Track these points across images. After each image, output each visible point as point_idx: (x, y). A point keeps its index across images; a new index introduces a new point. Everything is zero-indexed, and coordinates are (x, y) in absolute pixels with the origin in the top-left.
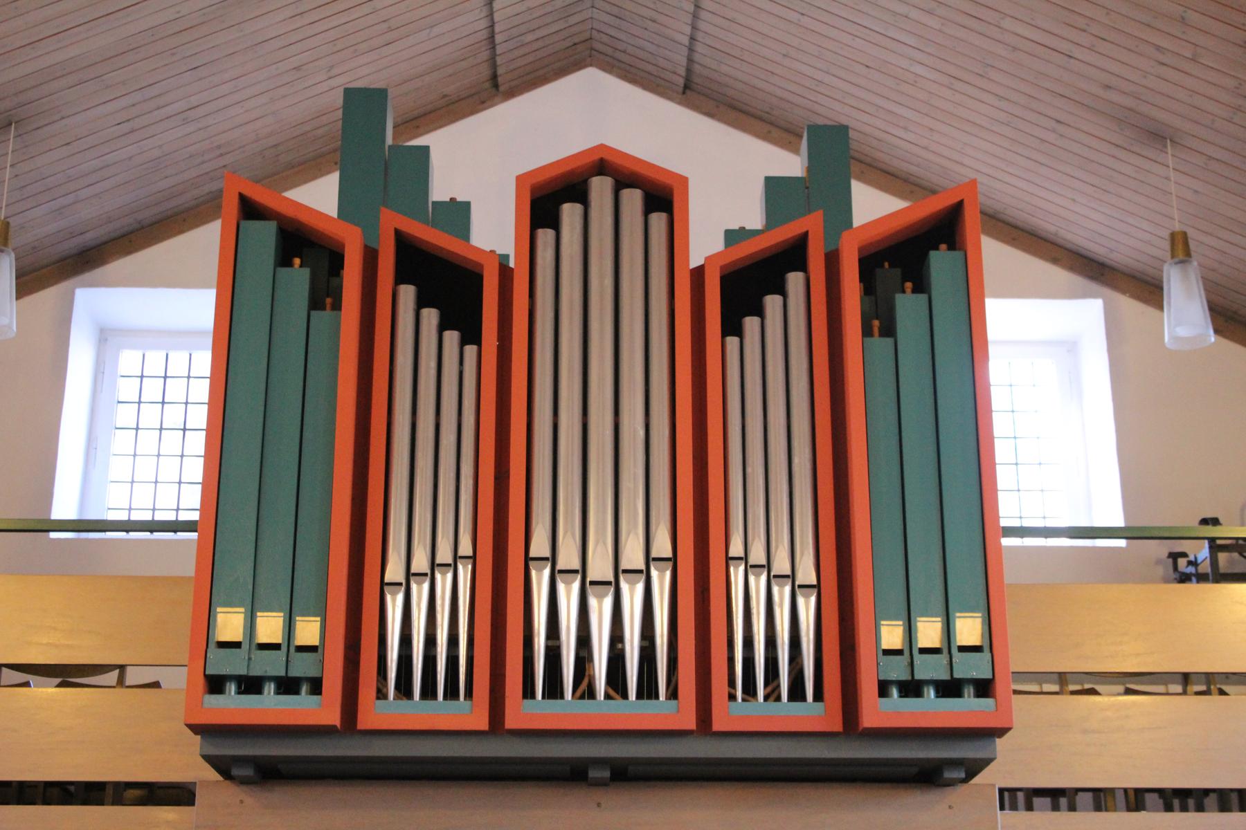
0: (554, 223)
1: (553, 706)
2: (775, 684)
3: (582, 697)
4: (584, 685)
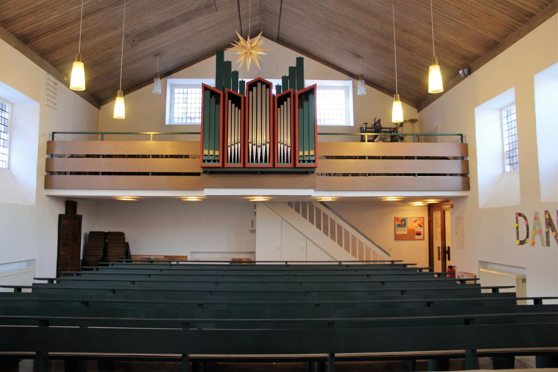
4: (257, 160)
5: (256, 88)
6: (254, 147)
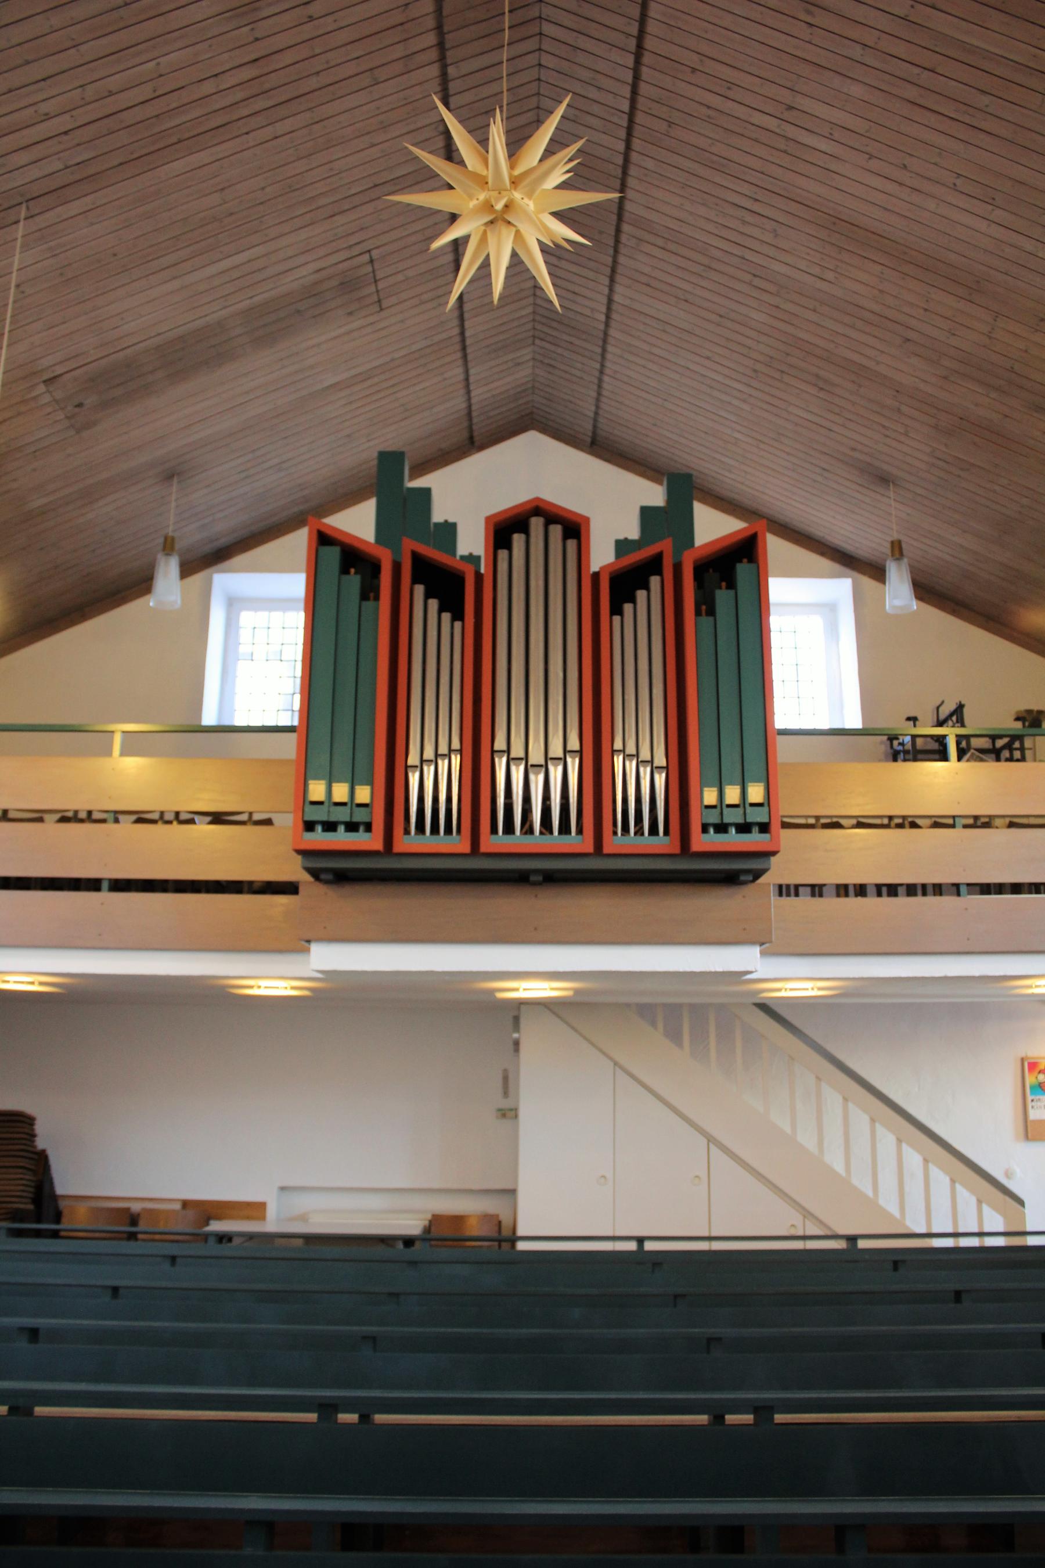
0: (508, 546)
1: (509, 839)
2: (641, 825)
3: (526, 833)
4: (527, 826)
5: (523, 536)
6: (518, 774)
